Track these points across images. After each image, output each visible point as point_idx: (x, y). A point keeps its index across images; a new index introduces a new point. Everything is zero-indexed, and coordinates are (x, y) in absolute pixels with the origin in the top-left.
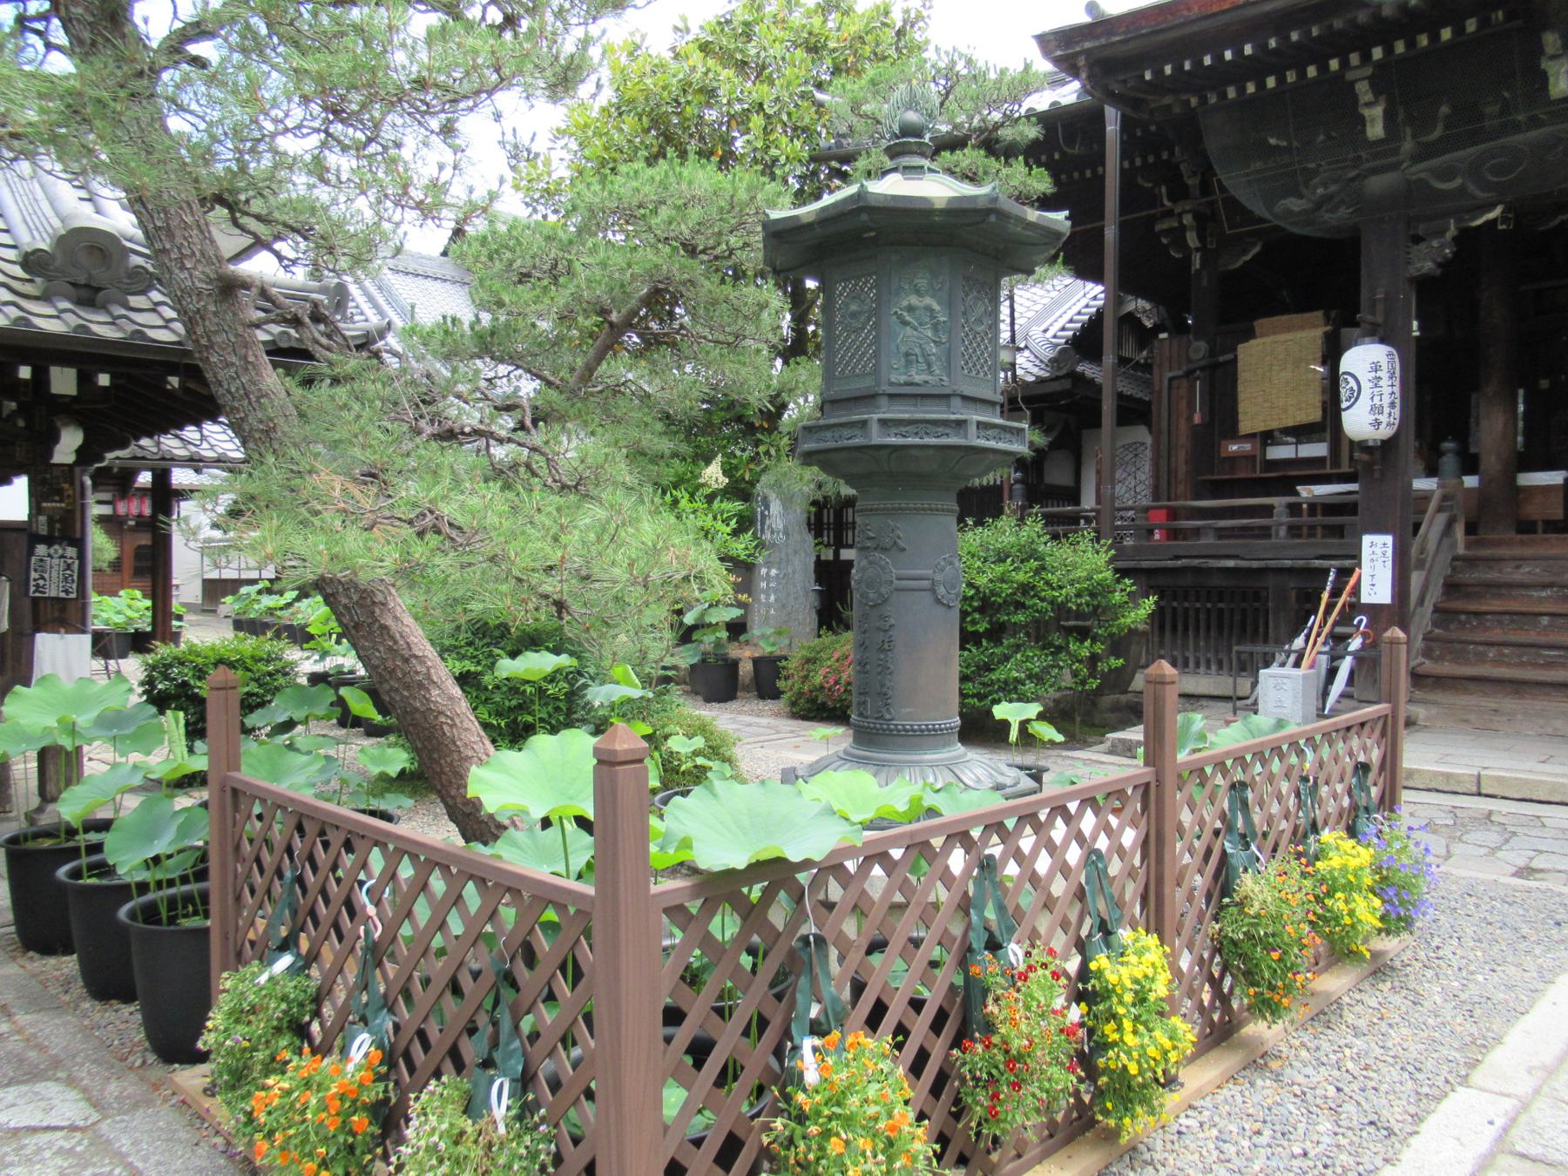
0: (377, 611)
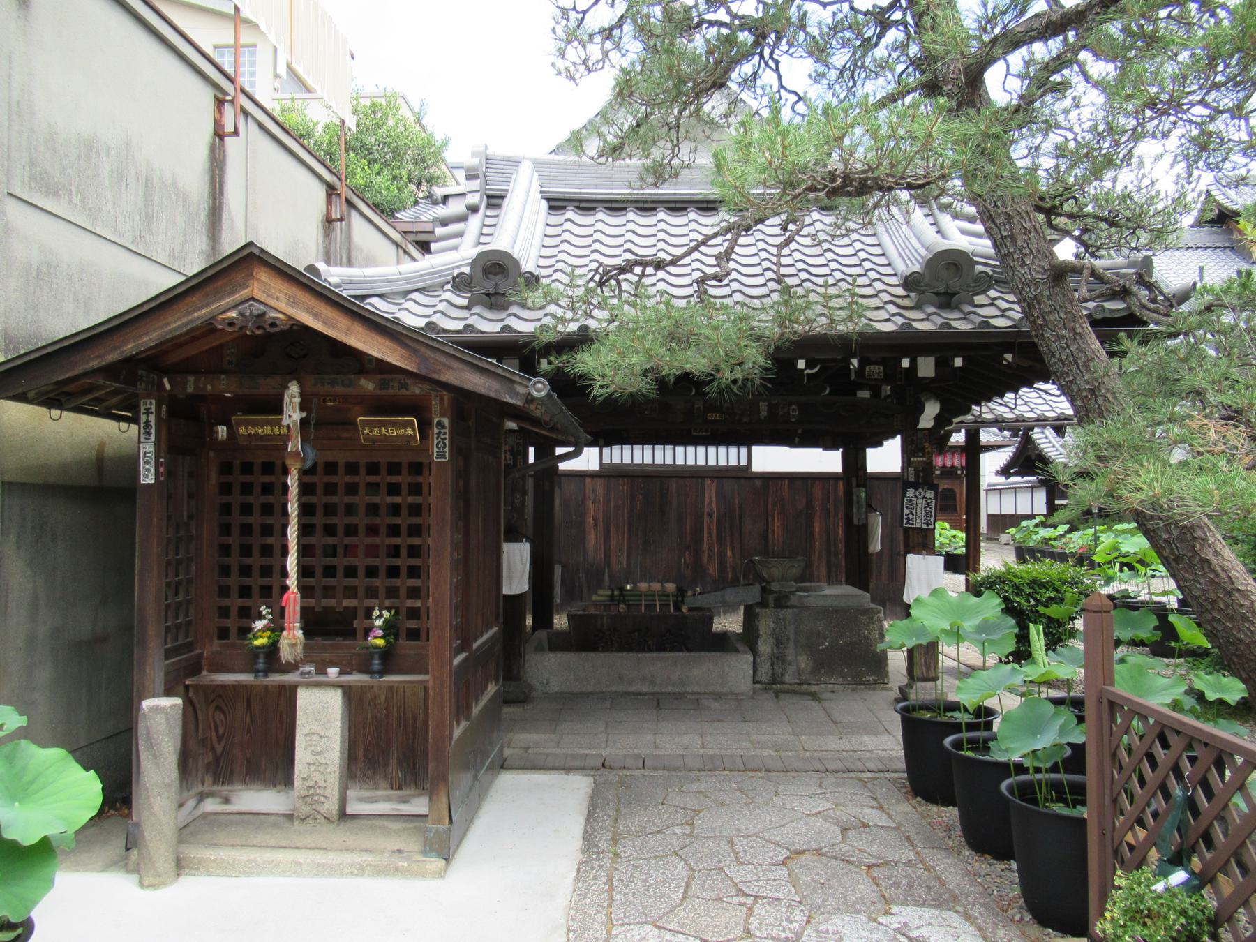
0: (1198, 546)
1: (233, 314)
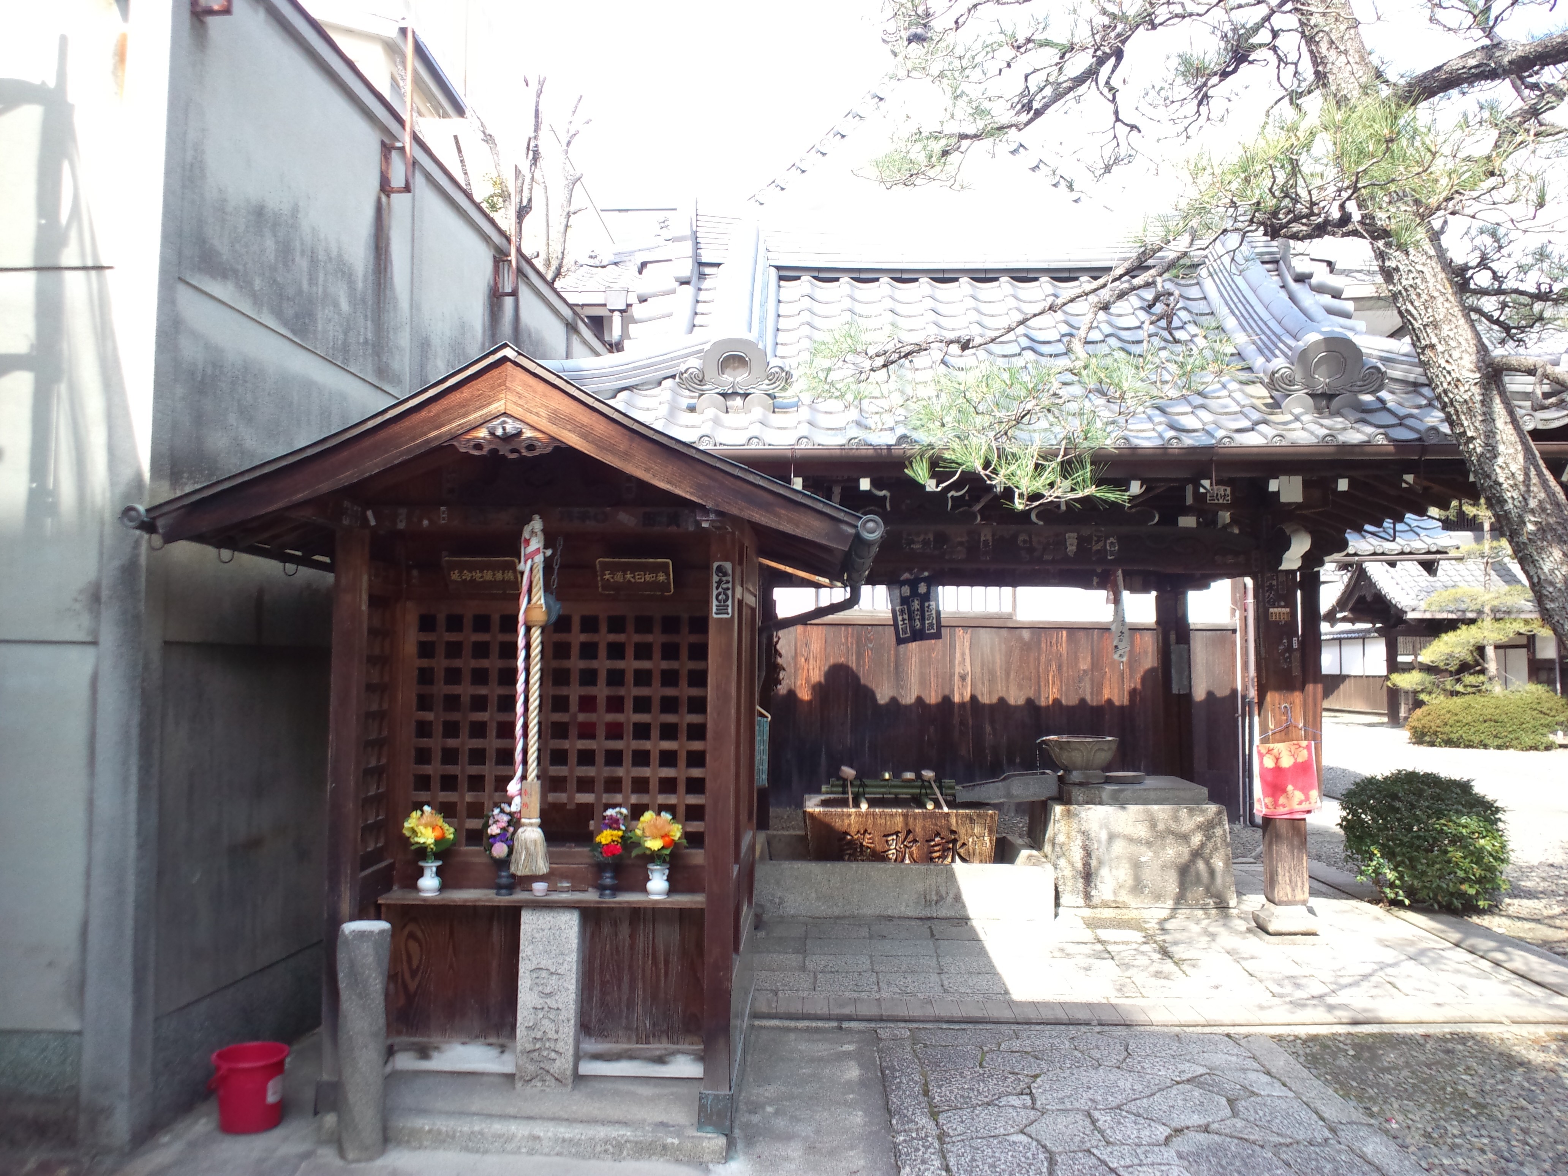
1: (483, 433)
